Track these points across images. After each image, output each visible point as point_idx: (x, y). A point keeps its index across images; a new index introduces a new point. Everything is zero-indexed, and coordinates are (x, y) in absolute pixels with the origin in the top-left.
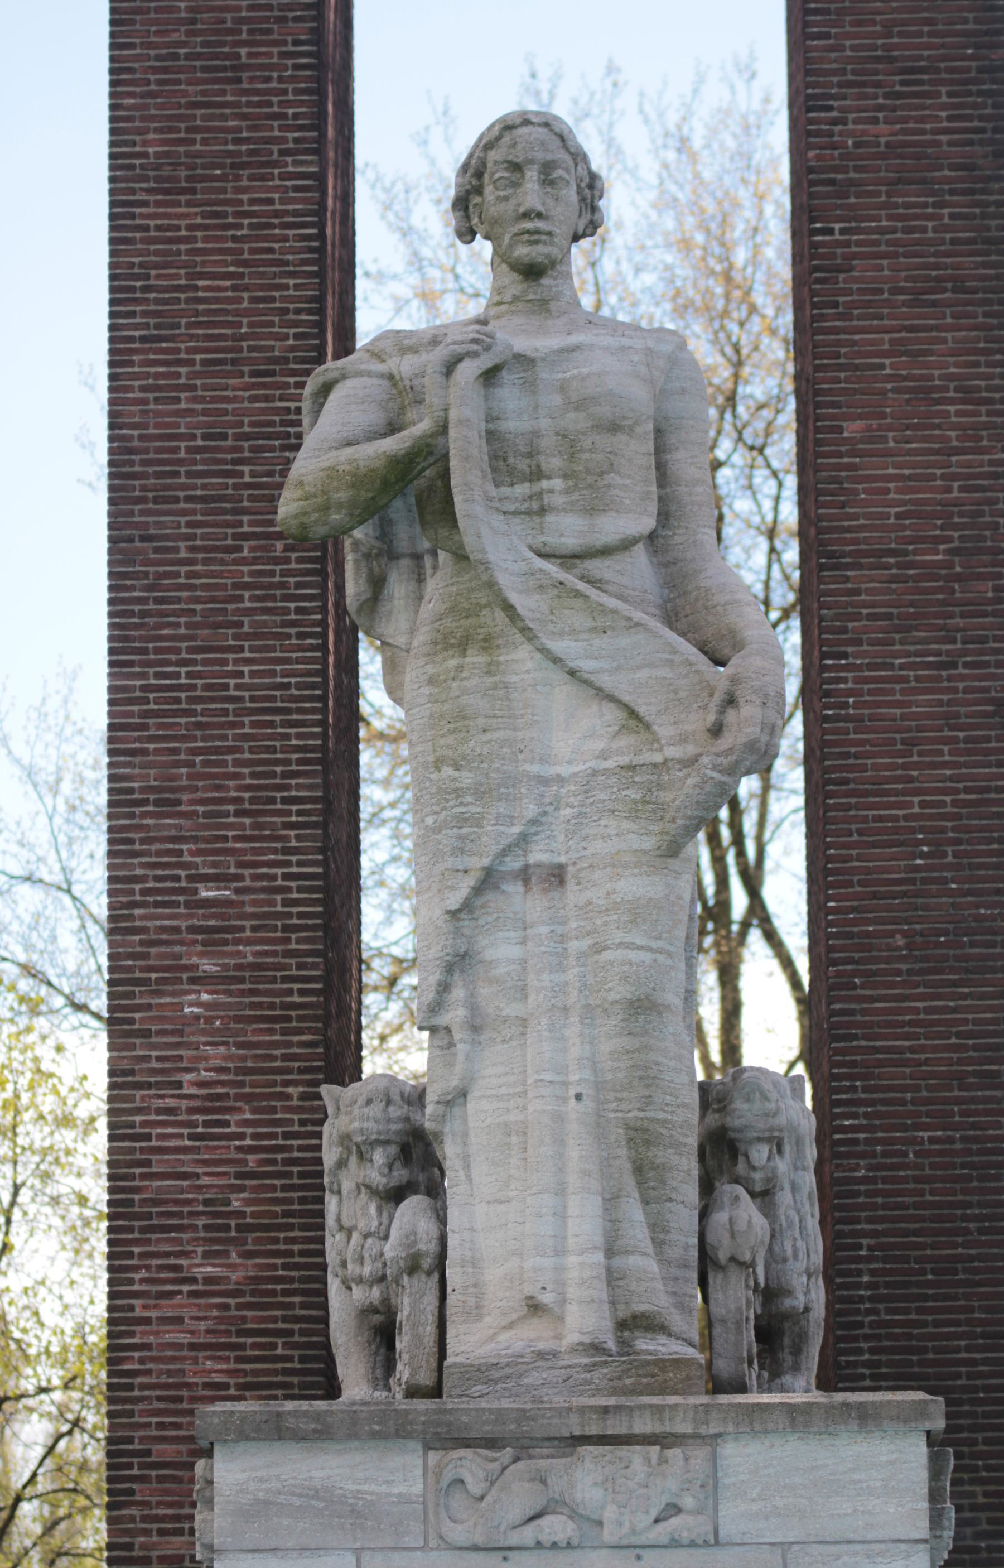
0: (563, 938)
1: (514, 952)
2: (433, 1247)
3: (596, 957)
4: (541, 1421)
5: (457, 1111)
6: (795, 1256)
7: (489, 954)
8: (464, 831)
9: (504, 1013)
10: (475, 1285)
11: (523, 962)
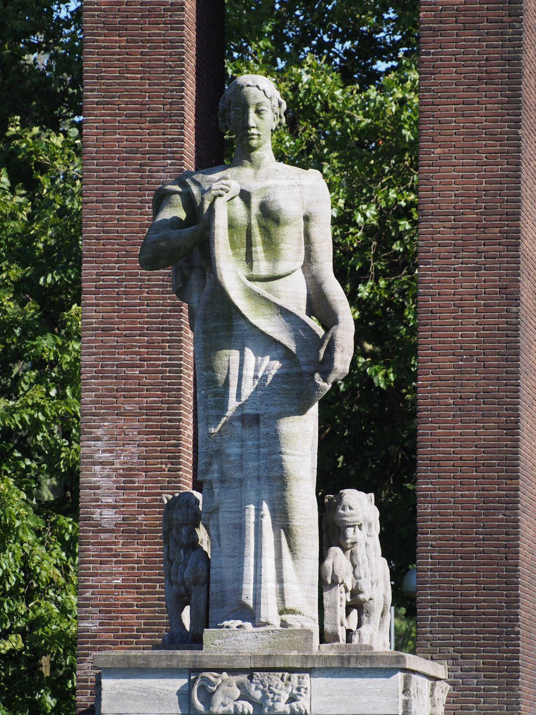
0: (258, 447)
1: (237, 451)
2: (204, 574)
3: (270, 457)
4: (237, 661)
5: (215, 515)
6: (365, 576)
7: (228, 451)
8: (217, 398)
10: (221, 592)
11: (241, 455)
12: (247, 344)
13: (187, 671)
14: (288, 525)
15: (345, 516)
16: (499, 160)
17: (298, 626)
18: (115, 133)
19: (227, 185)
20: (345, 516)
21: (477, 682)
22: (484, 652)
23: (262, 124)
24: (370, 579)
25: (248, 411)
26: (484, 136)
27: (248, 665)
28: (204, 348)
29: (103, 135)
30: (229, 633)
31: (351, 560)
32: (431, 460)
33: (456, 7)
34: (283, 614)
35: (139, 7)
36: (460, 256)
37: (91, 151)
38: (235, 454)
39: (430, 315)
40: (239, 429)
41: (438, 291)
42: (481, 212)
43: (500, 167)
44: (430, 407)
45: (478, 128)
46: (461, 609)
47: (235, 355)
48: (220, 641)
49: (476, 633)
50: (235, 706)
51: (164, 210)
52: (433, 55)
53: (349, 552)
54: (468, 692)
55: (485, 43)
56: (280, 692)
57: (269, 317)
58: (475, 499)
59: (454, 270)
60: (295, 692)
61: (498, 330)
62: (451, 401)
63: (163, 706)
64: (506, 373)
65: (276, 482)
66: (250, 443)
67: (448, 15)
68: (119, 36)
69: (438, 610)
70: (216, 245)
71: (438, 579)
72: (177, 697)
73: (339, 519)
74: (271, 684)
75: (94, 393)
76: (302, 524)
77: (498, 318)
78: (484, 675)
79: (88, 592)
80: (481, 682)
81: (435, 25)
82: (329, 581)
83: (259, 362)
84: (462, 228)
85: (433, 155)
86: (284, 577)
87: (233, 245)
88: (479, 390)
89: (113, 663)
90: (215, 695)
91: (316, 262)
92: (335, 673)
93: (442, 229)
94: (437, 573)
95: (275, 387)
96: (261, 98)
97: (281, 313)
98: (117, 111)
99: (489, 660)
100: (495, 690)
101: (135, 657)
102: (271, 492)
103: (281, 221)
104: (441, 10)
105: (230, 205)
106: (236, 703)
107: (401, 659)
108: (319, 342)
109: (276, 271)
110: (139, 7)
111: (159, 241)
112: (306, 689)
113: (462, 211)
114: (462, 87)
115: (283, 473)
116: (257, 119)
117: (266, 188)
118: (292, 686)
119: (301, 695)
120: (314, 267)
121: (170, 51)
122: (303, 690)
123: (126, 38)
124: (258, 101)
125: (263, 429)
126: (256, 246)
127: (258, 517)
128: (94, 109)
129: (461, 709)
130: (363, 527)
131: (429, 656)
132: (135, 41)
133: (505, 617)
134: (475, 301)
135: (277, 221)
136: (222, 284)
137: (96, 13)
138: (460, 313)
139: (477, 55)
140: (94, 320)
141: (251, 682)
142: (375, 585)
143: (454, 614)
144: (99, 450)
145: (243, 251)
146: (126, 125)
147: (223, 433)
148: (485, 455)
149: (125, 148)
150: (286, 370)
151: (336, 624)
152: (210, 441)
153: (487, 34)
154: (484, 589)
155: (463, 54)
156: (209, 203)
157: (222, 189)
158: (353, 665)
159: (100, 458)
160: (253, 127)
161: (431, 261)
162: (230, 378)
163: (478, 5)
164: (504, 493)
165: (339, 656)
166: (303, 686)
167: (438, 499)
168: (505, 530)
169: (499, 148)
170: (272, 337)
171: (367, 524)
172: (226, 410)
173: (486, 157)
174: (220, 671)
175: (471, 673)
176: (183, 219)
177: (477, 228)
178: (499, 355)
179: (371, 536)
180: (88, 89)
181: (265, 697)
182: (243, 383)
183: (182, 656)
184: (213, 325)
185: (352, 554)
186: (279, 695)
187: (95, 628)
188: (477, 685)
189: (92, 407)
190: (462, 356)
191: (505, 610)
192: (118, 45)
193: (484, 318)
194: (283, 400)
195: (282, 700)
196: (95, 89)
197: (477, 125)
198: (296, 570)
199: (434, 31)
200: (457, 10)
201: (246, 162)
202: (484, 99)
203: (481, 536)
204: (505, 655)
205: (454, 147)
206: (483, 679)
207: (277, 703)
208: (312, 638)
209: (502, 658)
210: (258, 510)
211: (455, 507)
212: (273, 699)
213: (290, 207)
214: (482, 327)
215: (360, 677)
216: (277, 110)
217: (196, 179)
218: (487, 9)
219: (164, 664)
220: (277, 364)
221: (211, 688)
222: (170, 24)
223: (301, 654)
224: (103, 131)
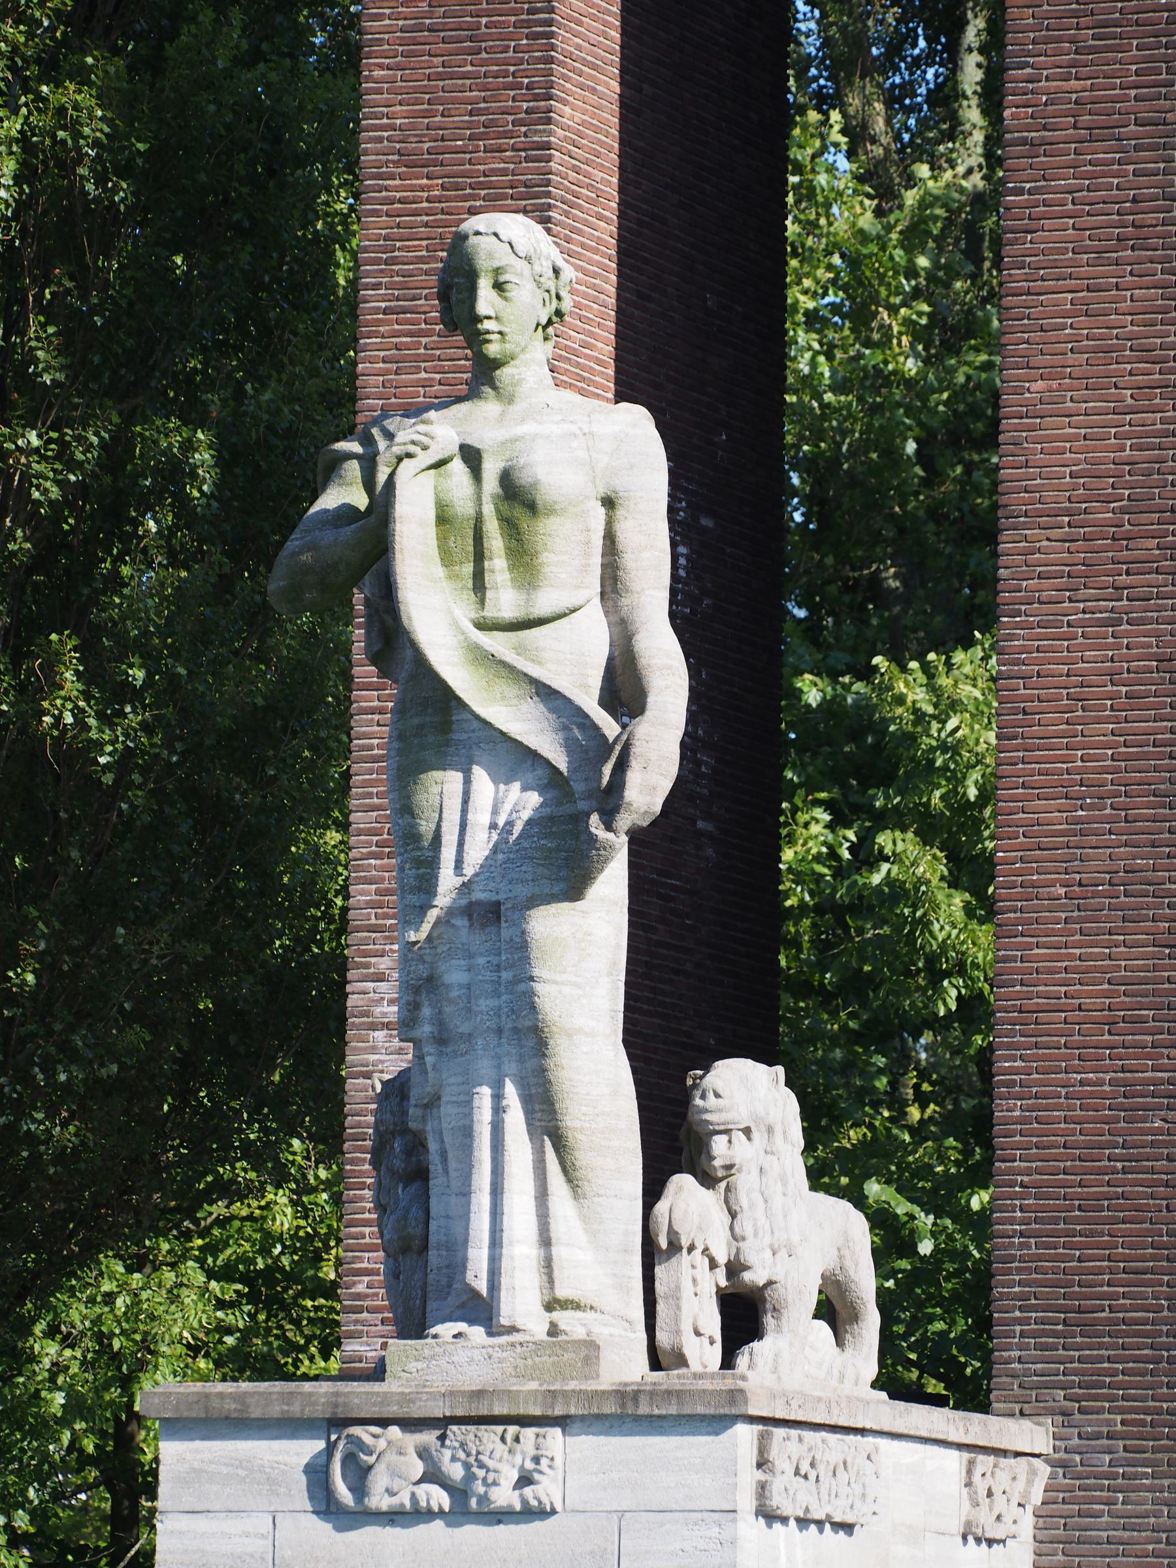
2: (419, 1231)
4: (418, 1403)
6: (756, 1235)
8: (421, 871)
9: (460, 1030)
10: (448, 1267)
11: (468, 987)
12: (477, 759)
13: (325, 1424)
14: (557, 1128)
15: (706, 1111)
16: (1157, 401)
17: (579, 1333)
18: (418, 370)
19: (426, 435)
20: (706, 1111)
21: (1110, 1461)
22: (1123, 1399)
23: (509, 310)
24: (767, 1240)
25: (479, 895)
26: (1128, 353)
27: (439, 1410)
28: (398, 769)
29: (396, 374)
30: (437, 1349)
31: (727, 1202)
32: (1021, 1012)
33: (1074, 96)
34: (555, 1309)
35: (467, 118)
36: (1080, 597)
37: (372, 405)
38: (459, 985)
39: (1020, 716)
40: (464, 932)
41: (1037, 668)
42: (1120, 508)
43: (1159, 415)
44: (1019, 904)
45: (1117, 338)
46: (1079, 1312)
47: (452, 780)
48: (420, 1365)
49: (1109, 1362)
50: (413, 1494)
51: (328, 491)
52: (1030, 194)
53: (723, 1185)
54: (1093, 1481)
55: (1131, 167)
56: (499, 1466)
57: (515, 702)
58: (1107, 1088)
59: (1069, 625)
60: (529, 1465)
61: (1154, 746)
62: (1062, 891)
63: (278, 1495)
64: (1169, 832)
65: (527, 1042)
66: (481, 961)
67: (1057, 114)
68: (428, 178)
69: (1034, 1315)
70: (398, 555)
71: (1034, 1251)
72: (304, 1478)
73: (696, 1117)
74: (480, 1449)
75: (374, 887)
76: (587, 1125)
77: (1155, 721)
78: (1125, 1446)
79: (360, 1282)
80: (1117, 1460)
81: (1033, 134)
82: (663, 1243)
83: (501, 794)
84: (1085, 540)
85: (1027, 395)
86: (552, 1235)
87: (447, 557)
88: (1115, 868)
89: (177, 1408)
90: (373, 1472)
91: (627, 591)
92: (612, 1427)
93: (1045, 543)
94: (1032, 1240)
95: (525, 845)
96: (503, 256)
97: (538, 694)
98: (423, 326)
99: (1134, 1416)
100: (1145, 1476)
101: (221, 1395)
102: (521, 1060)
103: (540, 506)
104: (1046, 104)
105: (440, 475)
106: (415, 1489)
107: (738, 1397)
108: (603, 747)
109: (531, 609)
110: (467, 118)
111: (301, 553)
112: (552, 1459)
113: (1084, 506)
114: (1086, 256)
115: (537, 1019)
116: (498, 301)
117: (514, 440)
118: (523, 1453)
119: (541, 1472)
120: (624, 601)
121: (524, 203)
122: (544, 1462)
123: (440, 181)
124: (496, 264)
125: (506, 932)
126: (491, 559)
127: (495, 1114)
128: (379, 323)
129: (1079, 1516)
130: (755, 1135)
131: (1017, 1407)
132: (457, 187)
133: (1165, 1328)
134: (1109, 688)
135: (532, 507)
136: (413, 636)
137: (386, 134)
138: (1080, 713)
139: (1115, 192)
140: (376, 741)
141: (443, 1445)
142: (783, 1253)
143: (1065, 1322)
144: (383, 999)
145: (468, 569)
146: (438, 352)
147: (436, 942)
148: (1127, 999)
149: (436, 397)
150: (549, 809)
151: (678, 1332)
152: (412, 959)
153: (1136, 148)
154: (1124, 1272)
155: (1089, 191)
156: (388, 471)
157: (413, 443)
158: (643, 1410)
159: (384, 1015)
160: (489, 318)
161: (1023, 608)
162: (443, 829)
163: (1117, 91)
164: (1165, 1075)
165: (617, 1392)
166: (544, 1453)
167: (1034, 1090)
168: (1166, 1151)
169: (1157, 376)
170: (521, 743)
171: (763, 1129)
172: (434, 894)
173: (1132, 396)
174: (384, 1423)
175: (1098, 1442)
176: (362, 509)
177: (1113, 539)
178: (1155, 795)
179: (772, 1153)
180: (367, 284)
181: (470, 1477)
182: (467, 838)
183: (311, 1394)
184: (416, 721)
185: (728, 1189)
186: (495, 1471)
187: (374, 1354)
188: (1110, 1466)
189: (369, 914)
190: (1084, 798)
191: (1165, 1313)
192: (425, 194)
193: (1126, 722)
194: (540, 870)
195: (502, 1482)
196: (381, 283)
197: (1115, 331)
198: (585, 1219)
199: (1032, 145)
200: (1076, 103)
201: (487, 389)
202: (1129, 278)
203: (1119, 1165)
204: (1165, 1406)
205: (1070, 378)
206: (1122, 1454)
207: (494, 1489)
208: (598, 1358)
209: (1159, 1411)
210: (498, 1097)
211: (1068, 1105)
212: (484, 1479)
213: (556, 473)
214: (1122, 739)
215: (662, 1434)
216: (551, 284)
217: (389, 427)
218: (1136, 99)
219: (276, 1410)
220: (534, 799)
221: (365, 1458)
222: (524, 150)
223: (545, 1387)
224: (395, 366)
